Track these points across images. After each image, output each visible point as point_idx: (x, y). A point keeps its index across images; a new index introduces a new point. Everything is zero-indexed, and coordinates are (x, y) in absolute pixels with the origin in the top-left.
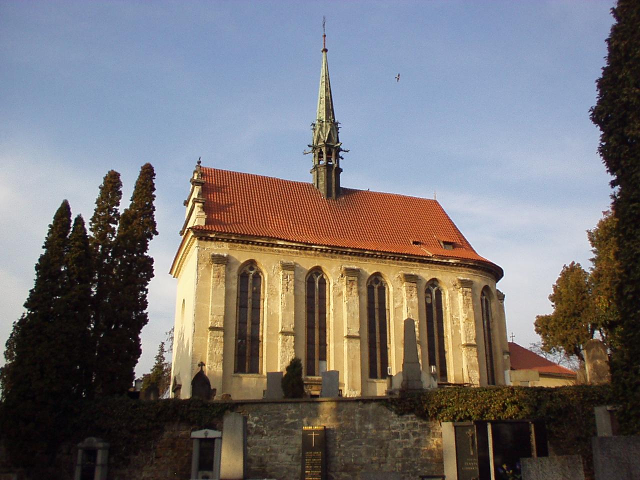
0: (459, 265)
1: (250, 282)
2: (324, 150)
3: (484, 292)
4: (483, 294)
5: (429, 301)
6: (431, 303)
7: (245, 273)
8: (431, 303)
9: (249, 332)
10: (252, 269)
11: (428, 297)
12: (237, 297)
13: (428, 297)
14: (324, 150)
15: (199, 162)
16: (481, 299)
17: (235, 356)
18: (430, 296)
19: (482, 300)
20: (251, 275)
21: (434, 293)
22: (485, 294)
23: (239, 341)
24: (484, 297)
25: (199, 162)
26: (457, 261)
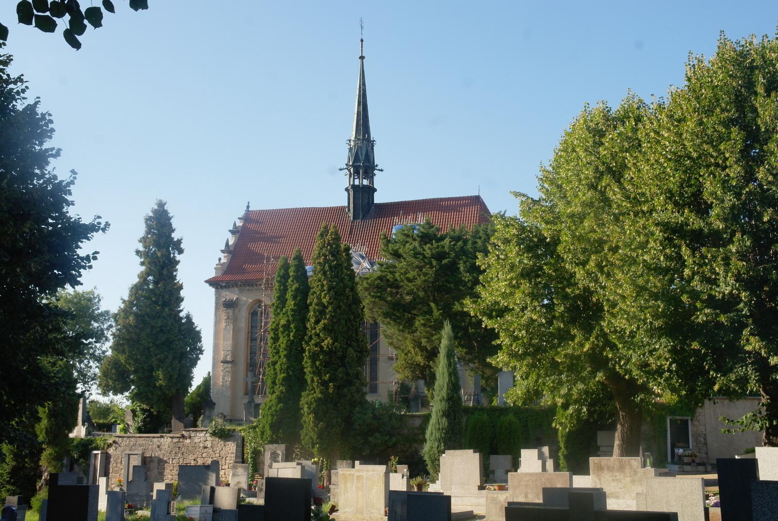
2: (352, 170)
12: (248, 333)
25: (248, 207)
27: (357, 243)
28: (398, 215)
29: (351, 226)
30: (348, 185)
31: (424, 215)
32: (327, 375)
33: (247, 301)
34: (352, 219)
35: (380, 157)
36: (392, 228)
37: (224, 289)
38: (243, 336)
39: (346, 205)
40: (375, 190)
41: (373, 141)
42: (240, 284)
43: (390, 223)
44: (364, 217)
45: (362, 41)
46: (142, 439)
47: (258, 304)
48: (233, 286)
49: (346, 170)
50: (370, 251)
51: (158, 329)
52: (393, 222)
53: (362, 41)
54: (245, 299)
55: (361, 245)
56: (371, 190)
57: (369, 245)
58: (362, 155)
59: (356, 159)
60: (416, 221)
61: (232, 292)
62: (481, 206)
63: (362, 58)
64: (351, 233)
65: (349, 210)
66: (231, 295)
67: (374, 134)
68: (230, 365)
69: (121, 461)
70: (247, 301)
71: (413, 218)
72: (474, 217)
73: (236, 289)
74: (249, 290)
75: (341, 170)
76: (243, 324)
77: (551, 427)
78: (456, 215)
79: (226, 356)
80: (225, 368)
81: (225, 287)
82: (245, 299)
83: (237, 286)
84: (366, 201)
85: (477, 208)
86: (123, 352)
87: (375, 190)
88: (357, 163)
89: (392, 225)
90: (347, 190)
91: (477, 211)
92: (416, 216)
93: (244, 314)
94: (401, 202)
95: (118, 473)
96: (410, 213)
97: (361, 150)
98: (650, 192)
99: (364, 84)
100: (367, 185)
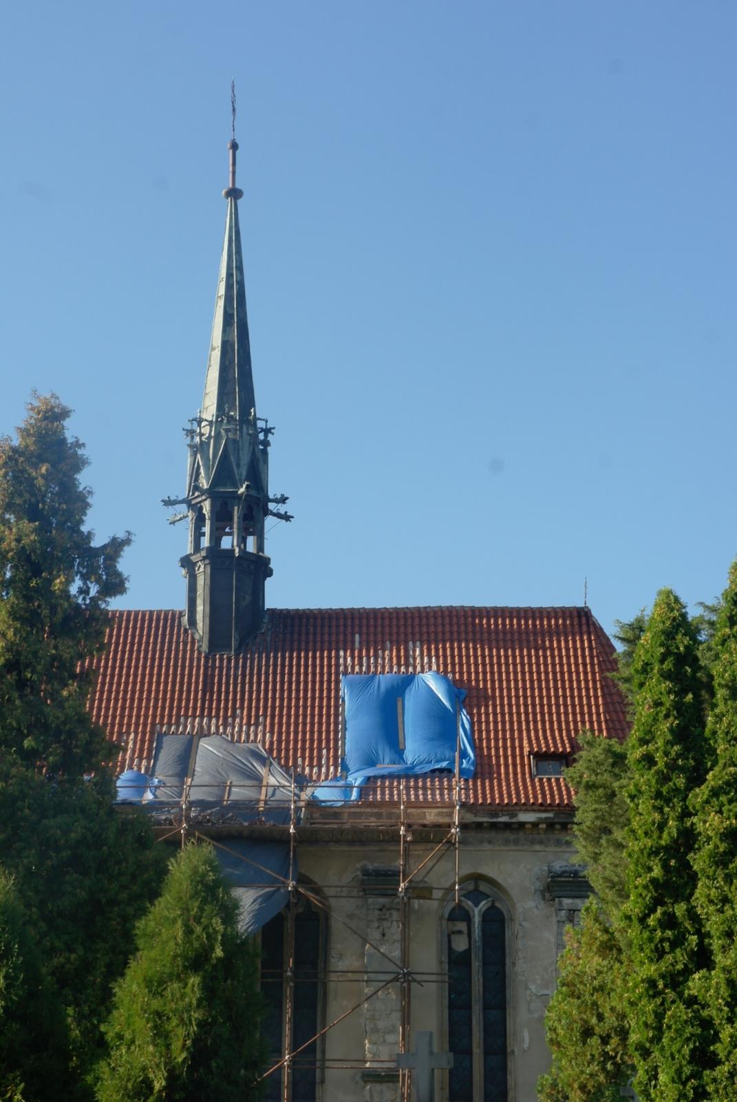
2: (207, 507)
5: (460, 944)
6: (468, 951)
8: (470, 949)
11: (460, 932)
13: (460, 932)
26: (544, 815)
27: (234, 716)
28: (348, 645)
29: (206, 668)
30: (189, 549)
31: (429, 650)
34: (205, 648)
36: (337, 682)
39: (181, 605)
41: (267, 431)
43: (329, 666)
44: (242, 646)
45: (234, 146)
49: (183, 508)
50: (279, 741)
51: (66, 854)
52: (337, 665)
53: (234, 146)
55: (249, 725)
56: (259, 568)
57: (272, 725)
58: (238, 466)
59: (224, 474)
60: (407, 666)
62: (597, 637)
63: (234, 194)
65: (192, 622)
67: (265, 408)
71: (399, 657)
72: (116, 700)
75: (169, 503)
78: (322, 658)
84: (248, 598)
85: (590, 641)
86: (628, 723)
88: (225, 486)
89: (337, 674)
90: (187, 562)
91: (591, 648)
92: (406, 651)
94: (352, 611)
96: (383, 642)
97: (237, 451)
98: (151, 772)
99: (240, 268)
100: (252, 554)
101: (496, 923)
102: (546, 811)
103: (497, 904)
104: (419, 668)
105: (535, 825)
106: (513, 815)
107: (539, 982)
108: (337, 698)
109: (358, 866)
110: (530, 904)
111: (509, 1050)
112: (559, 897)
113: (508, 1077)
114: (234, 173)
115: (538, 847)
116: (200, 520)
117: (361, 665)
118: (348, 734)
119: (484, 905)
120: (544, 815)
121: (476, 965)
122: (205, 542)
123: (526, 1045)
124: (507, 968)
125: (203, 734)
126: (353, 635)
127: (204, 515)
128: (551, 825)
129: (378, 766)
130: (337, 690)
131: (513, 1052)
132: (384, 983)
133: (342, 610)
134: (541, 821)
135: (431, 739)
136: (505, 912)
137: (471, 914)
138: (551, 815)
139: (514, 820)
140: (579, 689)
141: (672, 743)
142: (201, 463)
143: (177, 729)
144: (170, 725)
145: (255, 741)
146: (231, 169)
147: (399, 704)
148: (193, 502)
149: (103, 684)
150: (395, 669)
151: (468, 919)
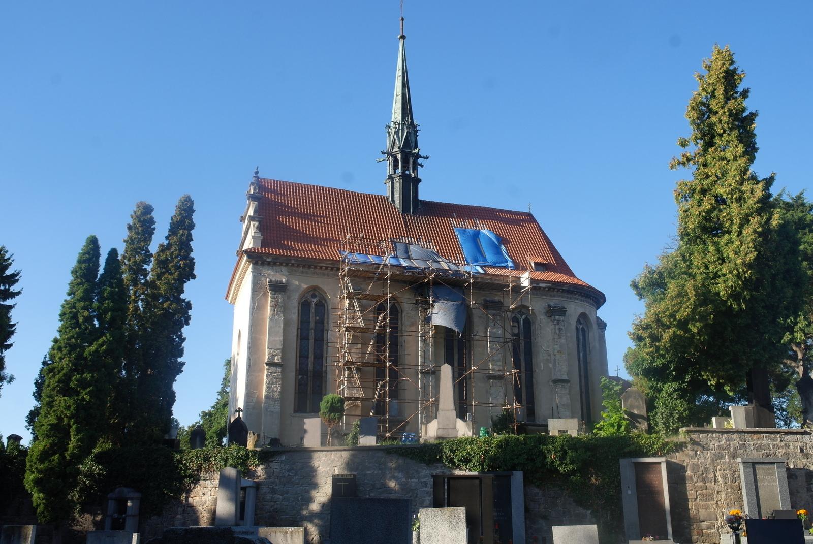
0: (552, 290)
1: (312, 310)
2: (399, 157)
3: (582, 321)
4: (579, 322)
7: (306, 301)
8: (519, 333)
9: (311, 366)
10: (314, 296)
11: (515, 326)
12: (298, 329)
13: (515, 326)
14: (399, 157)
15: (257, 173)
16: (576, 327)
17: (295, 393)
18: (517, 325)
19: (577, 329)
20: (313, 303)
21: (522, 322)
22: (582, 322)
23: (300, 377)
24: (581, 327)
25: (257, 173)
26: (548, 285)
32: (702, 374)
33: (299, 286)
34: (401, 211)
35: (423, 148)
37: (266, 267)
38: (293, 332)
39: (388, 193)
40: (420, 181)
42: (293, 262)
45: (403, 19)
46: (759, 436)
47: (311, 293)
48: (281, 264)
53: (403, 19)
54: (297, 283)
56: (417, 181)
61: (277, 272)
64: (406, 227)
66: (271, 275)
68: (279, 370)
69: (715, 476)
70: (299, 286)
73: (284, 269)
74: (302, 272)
76: (294, 316)
77: (180, 501)
79: (274, 356)
80: (271, 373)
81: (269, 263)
82: (297, 283)
83: (287, 265)
87: (420, 181)
90: (391, 178)
93: (294, 303)
95: (713, 499)
101: (528, 323)
102: (549, 283)
103: (528, 317)
104: (480, 228)
105: (544, 288)
106: (538, 284)
107: (546, 346)
108: (455, 236)
109: (482, 298)
110: (542, 317)
111: (534, 370)
112: (554, 315)
113: (534, 380)
114: (402, 29)
115: (544, 297)
116: (396, 161)
117: (460, 225)
118: (465, 251)
119: (524, 317)
120: (548, 285)
121: (522, 338)
122: (400, 170)
123: (542, 368)
124: (532, 340)
125: (411, 244)
126: (453, 213)
127: (398, 159)
128: (550, 288)
129: (479, 262)
130: (454, 233)
131: (535, 371)
132: (506, 331)
133: (473, 206)
134: (547, 287)
135: (495, 254)
136: (531, 320)
137: (520, 320)
138: (550, 285)
139: (538, 286)
140: (368, 233)
141: (705, 212)
142: (396, 139)
143: (400, 240)
144: (397, 239)
145: (430, 248)
146: (401, 28)
147: (478, 240)
148: (392, 154)
149: (410, 225)
150: (472, 228)
151: (519, 322)
